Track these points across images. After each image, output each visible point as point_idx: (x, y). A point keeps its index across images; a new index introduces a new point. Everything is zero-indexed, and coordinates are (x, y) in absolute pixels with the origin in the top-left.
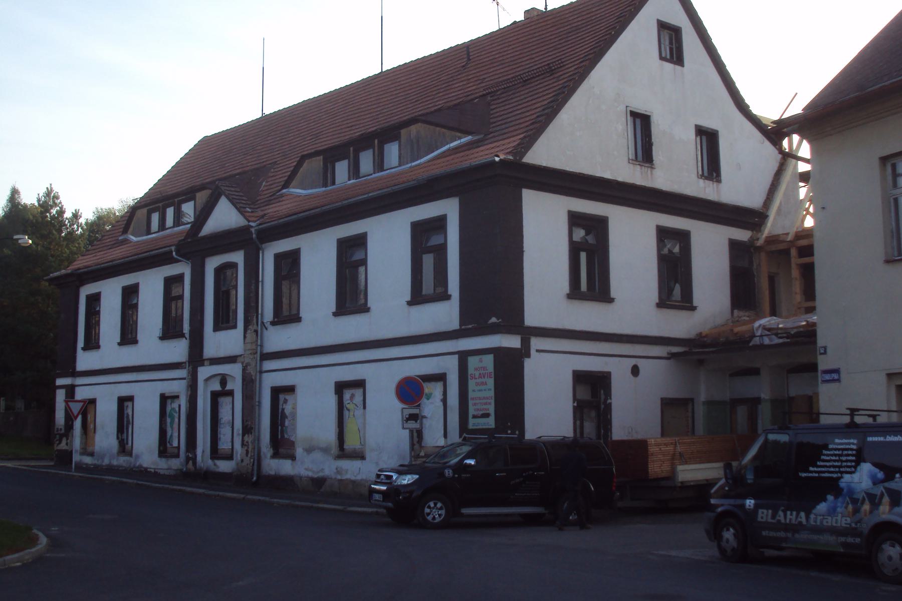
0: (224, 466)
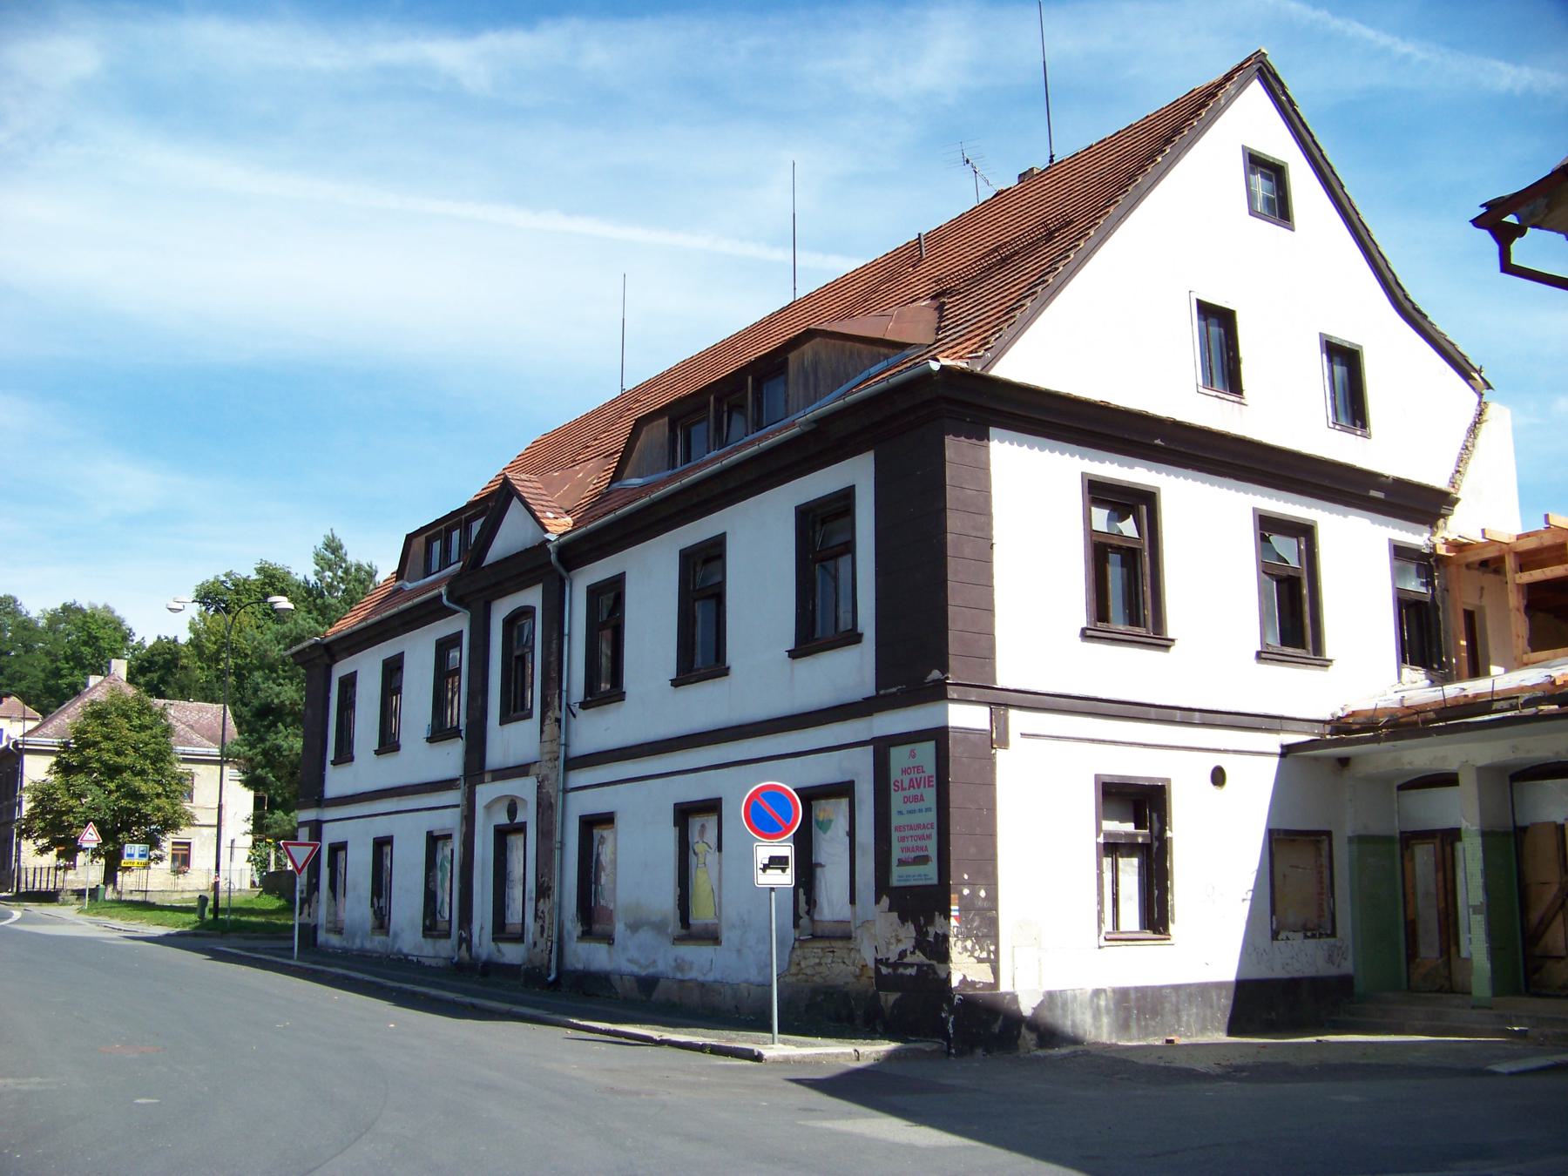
0: (512, 953)
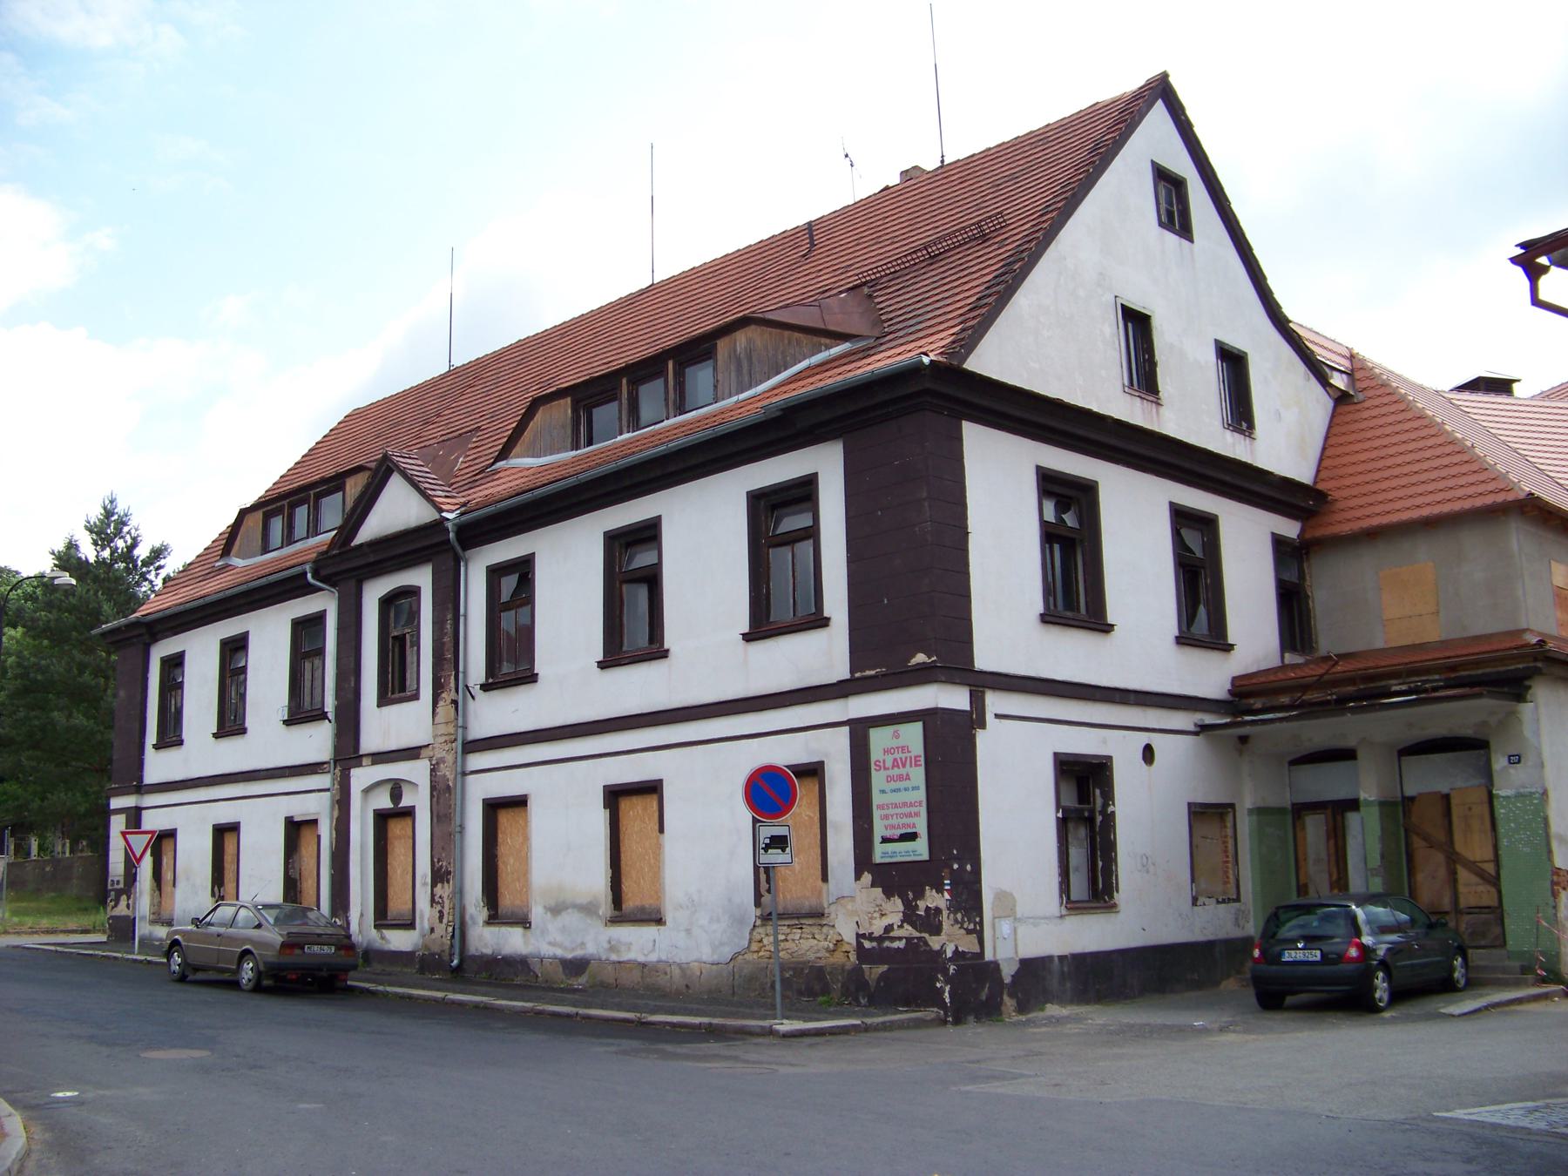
0: (399, 940)
